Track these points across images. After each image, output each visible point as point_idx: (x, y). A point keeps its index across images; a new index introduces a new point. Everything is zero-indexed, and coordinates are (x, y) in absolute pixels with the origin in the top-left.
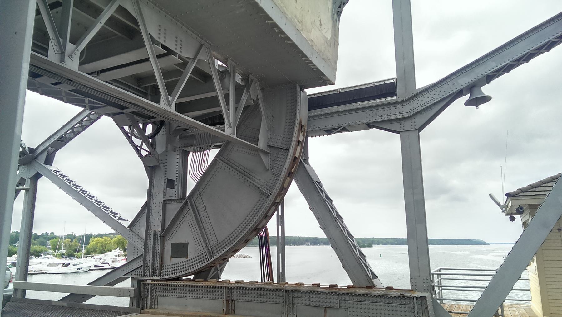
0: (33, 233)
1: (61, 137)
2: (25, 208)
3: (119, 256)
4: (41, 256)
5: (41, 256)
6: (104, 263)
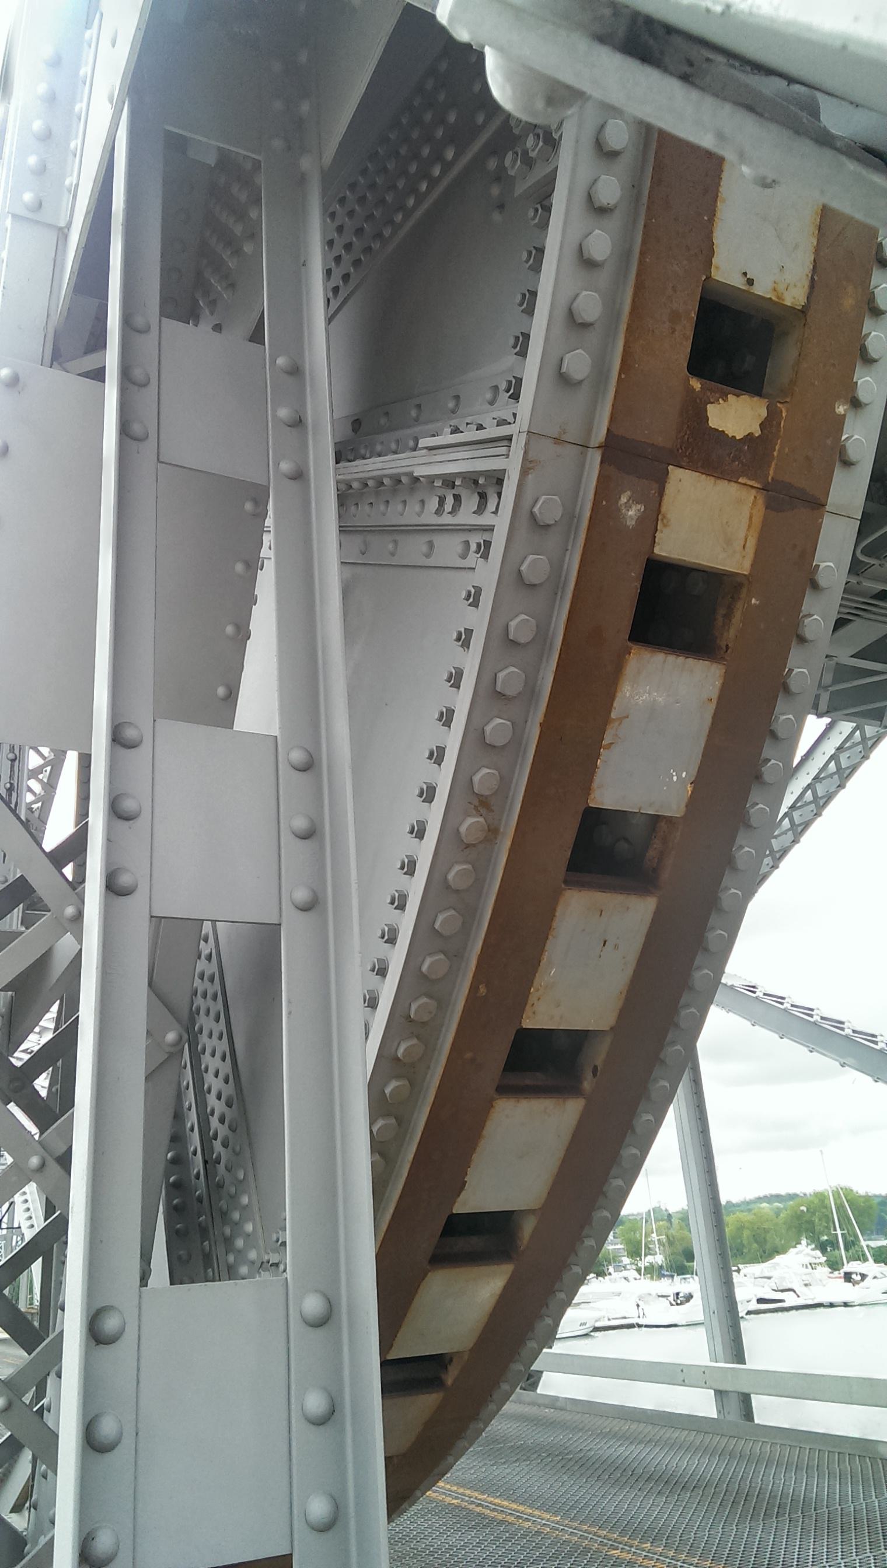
0: (804, 1242)
1: (326, 302)
2: (239, 1076)
3: (813, 1266)
4: (610, 1274)
5: (610, 1274)
6: (782, 1291)
